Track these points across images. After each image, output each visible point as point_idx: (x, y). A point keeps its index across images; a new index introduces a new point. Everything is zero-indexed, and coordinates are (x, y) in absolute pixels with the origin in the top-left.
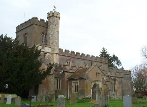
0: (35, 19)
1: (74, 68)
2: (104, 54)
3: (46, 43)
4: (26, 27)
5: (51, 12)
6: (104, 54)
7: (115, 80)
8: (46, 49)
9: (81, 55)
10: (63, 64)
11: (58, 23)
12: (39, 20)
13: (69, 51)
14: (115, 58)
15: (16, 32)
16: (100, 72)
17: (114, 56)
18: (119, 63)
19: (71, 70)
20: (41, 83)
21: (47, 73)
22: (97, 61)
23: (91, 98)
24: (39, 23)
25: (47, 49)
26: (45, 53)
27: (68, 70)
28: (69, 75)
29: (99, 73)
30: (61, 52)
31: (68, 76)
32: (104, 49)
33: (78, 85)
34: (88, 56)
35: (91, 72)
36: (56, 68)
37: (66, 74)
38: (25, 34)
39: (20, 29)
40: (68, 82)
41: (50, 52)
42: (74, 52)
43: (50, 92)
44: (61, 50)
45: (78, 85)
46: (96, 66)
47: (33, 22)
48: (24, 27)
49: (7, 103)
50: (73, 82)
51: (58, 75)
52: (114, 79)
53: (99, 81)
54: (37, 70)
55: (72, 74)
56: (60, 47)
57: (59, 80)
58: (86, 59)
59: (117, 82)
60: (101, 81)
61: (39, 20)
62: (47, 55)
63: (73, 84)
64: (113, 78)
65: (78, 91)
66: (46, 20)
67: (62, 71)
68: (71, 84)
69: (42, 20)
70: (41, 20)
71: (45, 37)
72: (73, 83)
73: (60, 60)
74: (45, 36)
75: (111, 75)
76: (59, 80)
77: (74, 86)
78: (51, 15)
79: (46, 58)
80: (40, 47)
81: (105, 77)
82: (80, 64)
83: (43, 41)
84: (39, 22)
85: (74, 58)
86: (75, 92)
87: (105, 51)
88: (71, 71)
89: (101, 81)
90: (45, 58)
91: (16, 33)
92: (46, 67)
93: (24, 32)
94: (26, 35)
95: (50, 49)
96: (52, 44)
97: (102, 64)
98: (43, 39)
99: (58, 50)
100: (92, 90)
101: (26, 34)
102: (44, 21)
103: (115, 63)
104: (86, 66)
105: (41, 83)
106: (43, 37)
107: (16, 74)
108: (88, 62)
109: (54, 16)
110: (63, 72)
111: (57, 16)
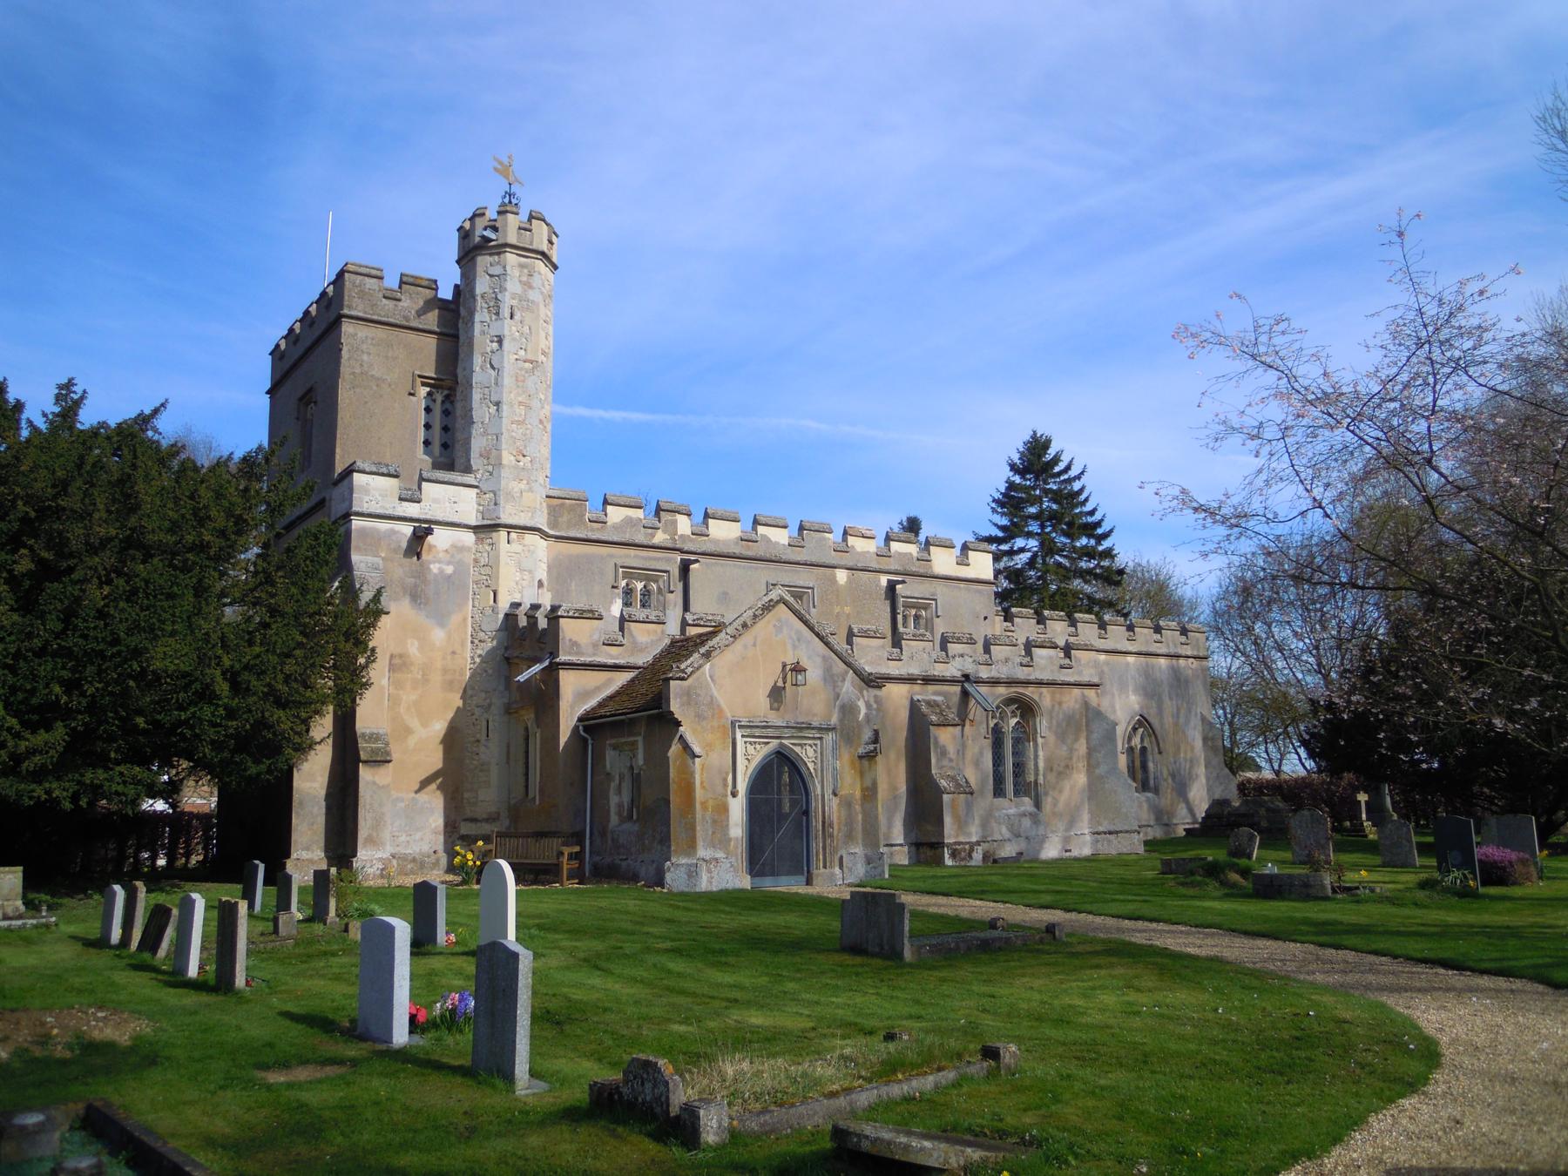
8: (435, 501)
15: (268, 386)
19: (614, 650)
23: (389, 785)
24: (390, 304)
27: (590, 650)
28: (598, 689)
30: (564, 519)
31: (583, 695)
37: (569, 682)
41: (473, 522)
43: (474, 820)
50: (615, 747)
52: (1009, 701)
55: (623, 678)
59: (1043, 725)
61: (392, 282)
62: (440, 539)
68: (599, 758)
72: (610, 755)
75: (984, 673)
77: (622, 778)
79: (435, 568)
96: (486, 455)
107: (1124, 810)
109: (5, 379)
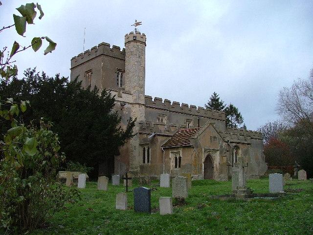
0: (104, 45)
1: (173, 129)
2: (215, 103)
3: (120, 85)
4: (88, 59)
5: (131, 33)
6: (215, 103)
7: (237, 148)
9: (181, 106)
10: (153, 123)
11: (143, 52)
12: (111, 47)
13: (161, 100)
14: (232, 110)
16: (216, 134)
17: (231, 106)
18: (238, 117)
19: (167, 132)
20: (118, 154)
21: (128, 135)
22: (207, 116)
25: (125, 98)
26: (123, 104)
28: (164, 141)
29: (215, 138)
32: (215, 94)
33: (180, 157)
34: (193, 107)
35: (202, 135)
36: (142, 129)
38: (87, 72)
39: (77, 63)
40: (163, 151)
42: (169, 102)
44: (148, 98)
45: (180, 157)
46: (211, 126)
47: (104, 52)
48: (85, 60)
49: (161, 186)
50: (172, 153)
51: (145, 140)
52: (235, 146)
53: (215, 151)
54: (113, 130)
56: (146, 94)
57: (146, 149)
58: (189, 112)
59: (240, 151)
60: (218, 150)
61: (111, 47)
62: (127, 106)
63: (172, 156)
64: (234, 144)
65: (180, 167)
66: (122, 46)
67: (153, 134)
69: (116, 48)
70: (115, 47)
71: (121, 77)
73: (147, 115)
74: (122, 75)
75: (232, 141)
76: (146, 149)
78: (131, 39)
80: (113, 93)
81: (224, 144)
82: (180, 121)
83: (118, 84)
84: (112, 50)
85: (170, 111)
86: (176, 169)
87: (217, 98)
88: (167, 133)
89: (218, 150)
90: (122, 113)
91: (70, 70)
92: (125, 128)
93: (85, 68)
94: (90, 73)
95: (131, 96)
97: (216, 121)
98: (118, 80)
99: (143, 98)
100: (203, 165)
101: (90, 71)
102: (119, 48)
103: (232, 119)
104: (190, 125)
105: (118, 154)
106: (118, 76)
108: (191, 118)
109: (137, 40)
110: (155, 136)
111: (141, 40)
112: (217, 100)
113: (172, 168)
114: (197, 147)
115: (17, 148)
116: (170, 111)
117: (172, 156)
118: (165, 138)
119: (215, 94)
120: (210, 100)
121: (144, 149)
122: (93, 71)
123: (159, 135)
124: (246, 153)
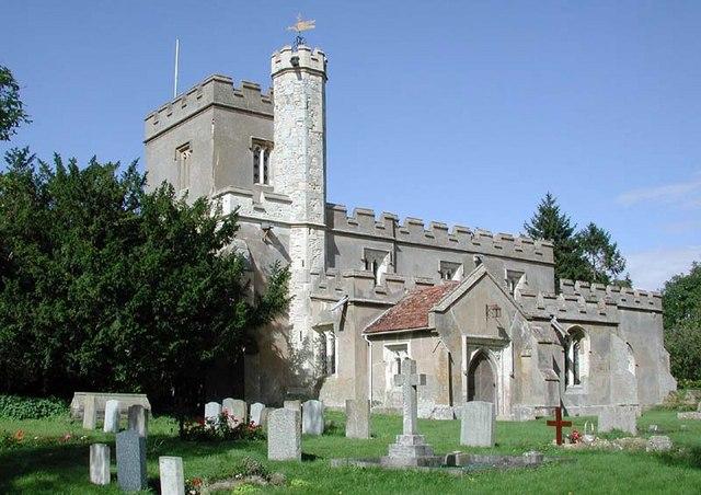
7: (577, 334)
17: (593, 229)
19: (379, 296)
32: (549, 197)
52: (571, 331)
67: (342, 301)
75: (562, 316)
94: (187, 152)
112: (555, 211)
113: (388, 387)
114: (447, 333)
115: (16, 330)
116: (619, 308)
117: (389, 356)
118: (373, 310)
119: (549, 197)
120: (538, 213)
121: (324, 337)
122: (193, 146)
123: (357, 304)
124: (602, 348)
